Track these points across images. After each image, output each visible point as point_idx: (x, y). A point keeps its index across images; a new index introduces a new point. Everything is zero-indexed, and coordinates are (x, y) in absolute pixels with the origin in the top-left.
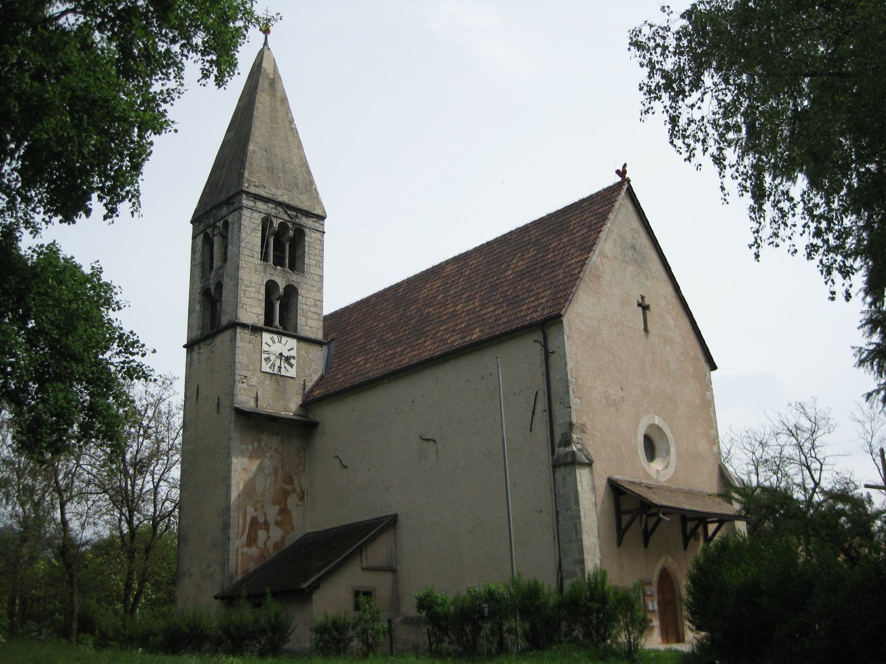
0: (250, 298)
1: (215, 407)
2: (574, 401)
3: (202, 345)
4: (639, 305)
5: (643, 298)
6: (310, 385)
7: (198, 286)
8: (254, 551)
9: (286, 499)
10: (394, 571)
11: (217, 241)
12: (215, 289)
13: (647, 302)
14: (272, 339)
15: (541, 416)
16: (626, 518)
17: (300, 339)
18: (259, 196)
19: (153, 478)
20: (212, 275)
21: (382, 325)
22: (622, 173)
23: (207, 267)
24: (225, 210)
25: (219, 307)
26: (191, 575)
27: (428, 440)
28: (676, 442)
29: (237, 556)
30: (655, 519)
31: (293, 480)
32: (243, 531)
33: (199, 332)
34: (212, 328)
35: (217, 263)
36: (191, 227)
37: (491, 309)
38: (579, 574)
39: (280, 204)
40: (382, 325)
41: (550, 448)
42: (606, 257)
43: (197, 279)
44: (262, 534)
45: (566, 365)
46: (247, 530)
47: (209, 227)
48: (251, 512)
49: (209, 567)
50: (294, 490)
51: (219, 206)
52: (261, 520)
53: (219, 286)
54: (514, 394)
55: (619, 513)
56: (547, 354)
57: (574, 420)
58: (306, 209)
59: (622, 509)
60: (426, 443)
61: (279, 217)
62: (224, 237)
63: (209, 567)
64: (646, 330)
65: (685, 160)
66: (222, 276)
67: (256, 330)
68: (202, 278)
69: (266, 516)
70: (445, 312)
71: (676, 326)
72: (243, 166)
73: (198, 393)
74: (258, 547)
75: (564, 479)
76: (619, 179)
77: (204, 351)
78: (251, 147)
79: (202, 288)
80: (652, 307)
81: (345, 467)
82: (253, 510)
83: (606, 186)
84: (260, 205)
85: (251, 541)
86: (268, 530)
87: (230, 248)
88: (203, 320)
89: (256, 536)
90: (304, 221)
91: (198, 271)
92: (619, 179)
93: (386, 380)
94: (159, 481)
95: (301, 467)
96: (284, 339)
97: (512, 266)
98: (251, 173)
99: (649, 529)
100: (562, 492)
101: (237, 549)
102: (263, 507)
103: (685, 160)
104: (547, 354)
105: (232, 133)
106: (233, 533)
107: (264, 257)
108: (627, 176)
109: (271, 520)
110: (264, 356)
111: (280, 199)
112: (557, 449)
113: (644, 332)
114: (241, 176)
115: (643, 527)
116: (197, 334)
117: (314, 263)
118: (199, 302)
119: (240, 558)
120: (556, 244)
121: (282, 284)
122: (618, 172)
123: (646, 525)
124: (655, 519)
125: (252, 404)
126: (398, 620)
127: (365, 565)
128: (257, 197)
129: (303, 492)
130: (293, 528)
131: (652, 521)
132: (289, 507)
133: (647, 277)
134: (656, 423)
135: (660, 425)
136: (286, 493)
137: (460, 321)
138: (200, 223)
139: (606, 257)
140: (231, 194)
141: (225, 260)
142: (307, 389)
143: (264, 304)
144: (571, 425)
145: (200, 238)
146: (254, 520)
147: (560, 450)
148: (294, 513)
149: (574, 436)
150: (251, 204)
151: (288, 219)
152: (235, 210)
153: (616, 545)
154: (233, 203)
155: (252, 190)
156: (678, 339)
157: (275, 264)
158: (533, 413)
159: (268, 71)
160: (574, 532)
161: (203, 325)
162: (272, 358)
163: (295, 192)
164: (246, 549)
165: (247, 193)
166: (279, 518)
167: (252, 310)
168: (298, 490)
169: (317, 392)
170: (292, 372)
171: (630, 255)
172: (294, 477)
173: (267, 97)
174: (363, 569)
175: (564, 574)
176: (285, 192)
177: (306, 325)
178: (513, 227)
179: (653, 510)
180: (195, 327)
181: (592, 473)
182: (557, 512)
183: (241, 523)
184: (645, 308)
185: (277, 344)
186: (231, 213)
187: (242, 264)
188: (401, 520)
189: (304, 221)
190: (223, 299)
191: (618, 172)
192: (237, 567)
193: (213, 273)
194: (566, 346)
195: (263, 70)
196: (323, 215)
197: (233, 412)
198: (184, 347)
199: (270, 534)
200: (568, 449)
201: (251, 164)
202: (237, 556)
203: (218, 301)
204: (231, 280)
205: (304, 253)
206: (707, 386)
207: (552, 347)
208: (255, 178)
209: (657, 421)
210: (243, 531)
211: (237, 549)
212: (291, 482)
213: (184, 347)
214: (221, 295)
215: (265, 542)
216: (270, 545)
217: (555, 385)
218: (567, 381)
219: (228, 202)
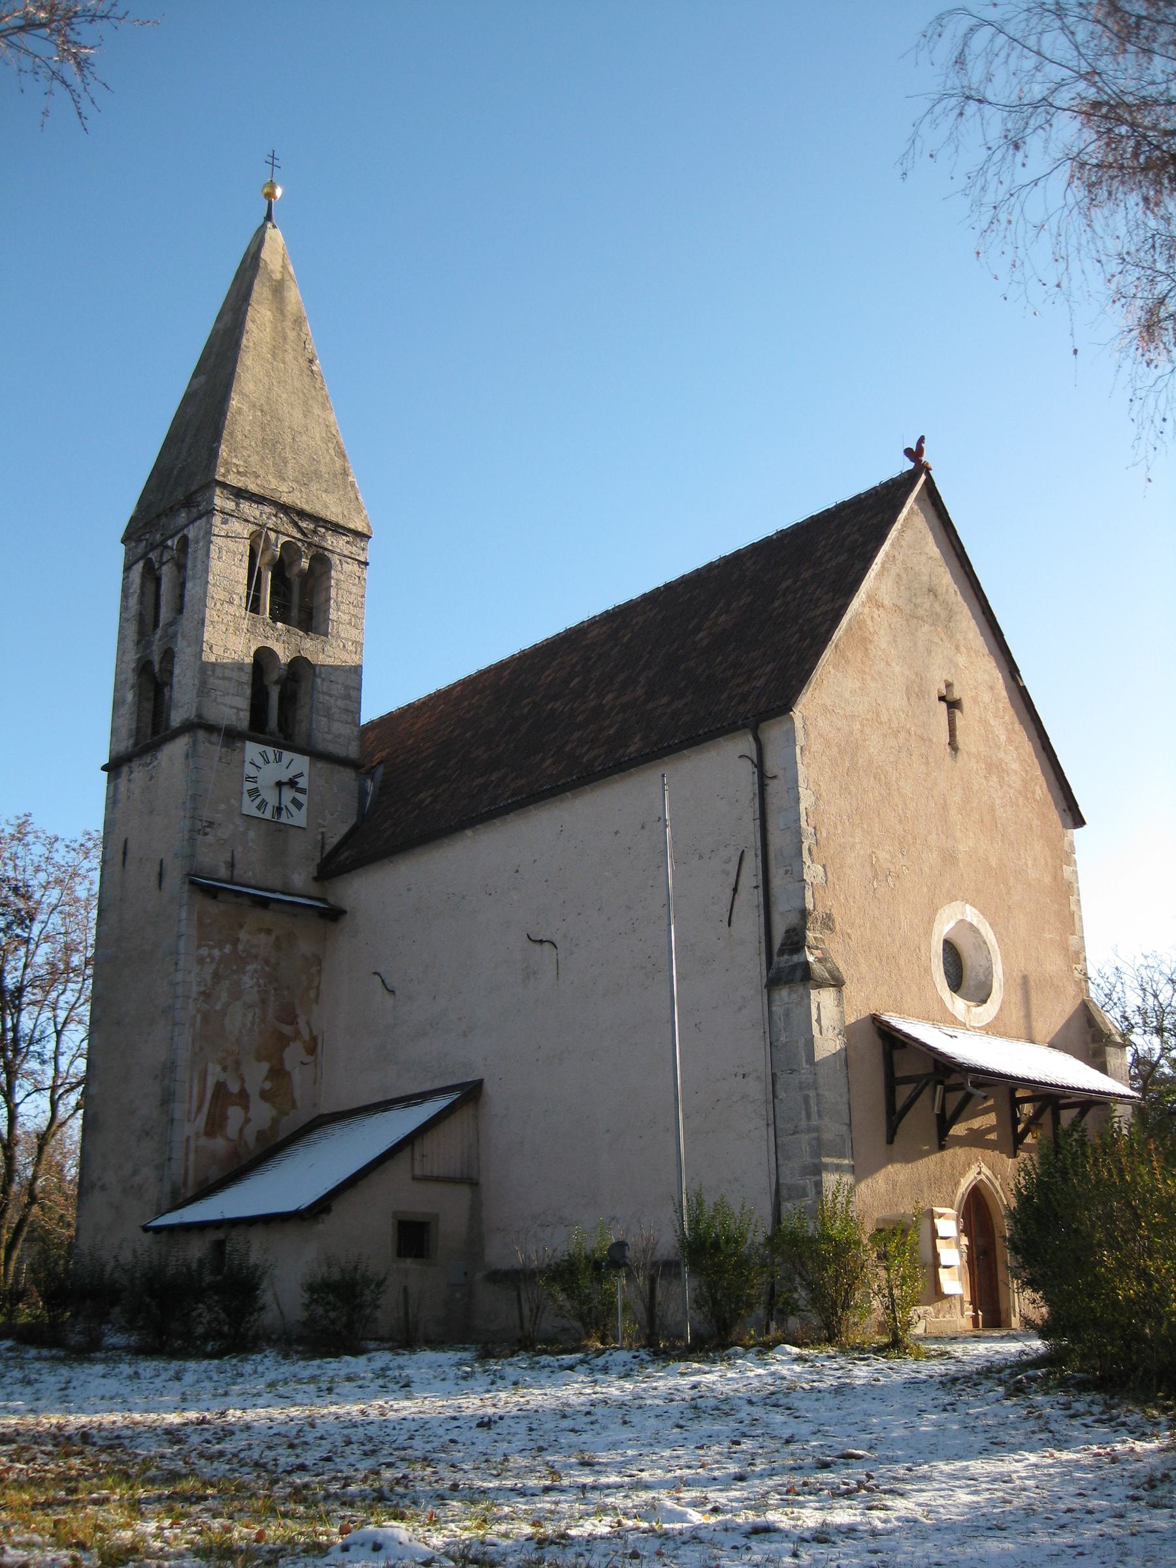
0: (224, 678)
1: (154, 879)
2: (812, 872)
3: (135, 764)
4: (942, 698)
5: (949, 685)
6: (333, 840)
7: (132, 656)
8: (219, 1144)
9: (282, 1050)
10: (473, 1183)
11: (167, 573)
12: (161, 662)
13: (957, 694)
14: (263, 755)
15: (749, 896)
16: (903, 1093)
17: (317, 755)
18: (247, 491)
19: (55, 1017)
20: (157, 636)
21: (468, 735)
22: (915, 454)
23: (149, 620)
24: (183, 517)
25: (167, 694)
26: (103, 1188)
27: (541, 942)
28: (1005, 956)
29: (187, 1154)
30: (960, 1095)
31: (296, 1016)
32: (200, 1108)
33: (131, 741)
34: (155, 732)
35: (165, 614)
36: (122, 548)
37: (664, 700)
38: (811, 1191)
39: (285, 509)
40: (468, 735)
41: (764, 957)
42: (879, 605)
43: (130, 644)
44: (235, 1114)
45: (797, 800)
46: (207, 1104)
48: (215, 1073)
49: (135, 1172)
50: (298, 1033)
51: (172, 511)
52: (234, 1088)
53: (169, 656)
54: (701, 857)
55: (891, 1082)
56: (763, 779)
57: (810, 906)
58: (334, 519)
59: (898, 1074)
60: (537, 947)
61: (284, 531)
62: (181, 567)
63: (135, 1172)
64: (953, 745)
67: (232, 737)
68: (138, 642)
69: (243, 1081)
70: (583, 708)
71: (1009, 740)
72: (217, 437)
73: (125, 853)
74: (228, 1139)
75: (787, 1015)
76: (910, 465)
77: (138, 773)
78: (235, 402)
79: (139, 659)
80: (966, 704)
81: (392, 992)
82: (218, 1068)
83: (885, 479)
84: (249, 509)
85: (215, 1125)
86: (246, 1108)
87: (189, 585)
88: (139, 720)
89: (225, 1118)
90: (335, 543)
91: (132, 629)
92: (910, 465)
93: (469, 833)
94: (65, 1023)
95: (312, 994)
96: (287, 755)
97: (708, 624)
98: (233, 450)
99: (949, 1114)
100: (783, 1039)
101: (188, 1138)
102: (238, 1064)
104: (763, 779)
105: (202, 379)
106: (179, 1110)
107: (254, 606)
108: (924, 459)
109: (253, 1091)
110: (249, 786)
111: (285, 499)
112: (775, 958)
113: (948, 749)
114: (213, 454)
115: (937, 1111)
116: (126, 744)
117: (346, 618)
118: (133, 687)
119: (192, 1157)
120: (789, 582)
121: (285, 656)
122: (908, 452)
123: (943, 1108)
124: (960, 1095)
125: (223, 872)
126: (479, 1276)
127: (418, 1171)
128: (240, 494)
129: (314, 1039)
130: (294, 1106)
131: (954, 1099)
132: (288, 1067)
133: (957, 648)
134: (969, 919)
135: (975, 923)
136: (283, 1041)
137: (607, 723)
138: (139, 540)
139: (879, 605)
140: (194, 488)
141: (180, 609)
142: (328, 848)
143: (248, 692)
144: (804, 914)
145: (139, 567)
146: (220, 1087)
147: (783, 961)
148: (297, 1077)
149: (810, 935)
150: (230, 505)
151: (299, 536)
152: (200, 517)
153: (883, 1140)
155: (233, 480)
156: (1015, 766)
157: (275, 618)
158: (735, 890)
159: (271, 267)
160: (803, 1114)
161: (138, 728)
163: (314, 487)
164: (203, 1141)
165: (224, 485)
166: (268, 1085)
167: (228, 700)
168: (306, 1037)
169: (346, 854)
170: (299, 818)
171: (927, 606)
172: (299, 1011)
173: (269, 313)
174: (414, 1178)
175: (784, 1193)
176: (295, 485)
178: (713, 557)
179: (954, 1080)
180: (124, 732)
181: (840, 1002)
182: (774, 1075)
183: (196, 1090)
184: (953, 705)
185: (273, 765)
186: (192, 522)
187: (210, 614)
188: (488, 1087)
189: (335, 543)
190: (175, 680)
191: (908, 452)
192: (186, 1173)
193: (159, 632)
194: (799, 765)
195: (262, 264)
196: (365, 531)
197: (186, 887)
198: (104, 768)
199: (251, 1114)
200: (796, 958)
201: (231, 434)
202: (187, 1154)
203: (166, 684)
204: (189, 646)
205: (328, 599)
206: (1066, 856)
207: (771, 766)
208: (238, 459)
209: (972, 915)
210: (200, 1108)
211: (188, 1138)
212: (292, 1020)
213: (104, 768)
214: (171, 673)
215: (241, 1130)
217: (777, 839)
218: (798, 833)
219: (189, 502)
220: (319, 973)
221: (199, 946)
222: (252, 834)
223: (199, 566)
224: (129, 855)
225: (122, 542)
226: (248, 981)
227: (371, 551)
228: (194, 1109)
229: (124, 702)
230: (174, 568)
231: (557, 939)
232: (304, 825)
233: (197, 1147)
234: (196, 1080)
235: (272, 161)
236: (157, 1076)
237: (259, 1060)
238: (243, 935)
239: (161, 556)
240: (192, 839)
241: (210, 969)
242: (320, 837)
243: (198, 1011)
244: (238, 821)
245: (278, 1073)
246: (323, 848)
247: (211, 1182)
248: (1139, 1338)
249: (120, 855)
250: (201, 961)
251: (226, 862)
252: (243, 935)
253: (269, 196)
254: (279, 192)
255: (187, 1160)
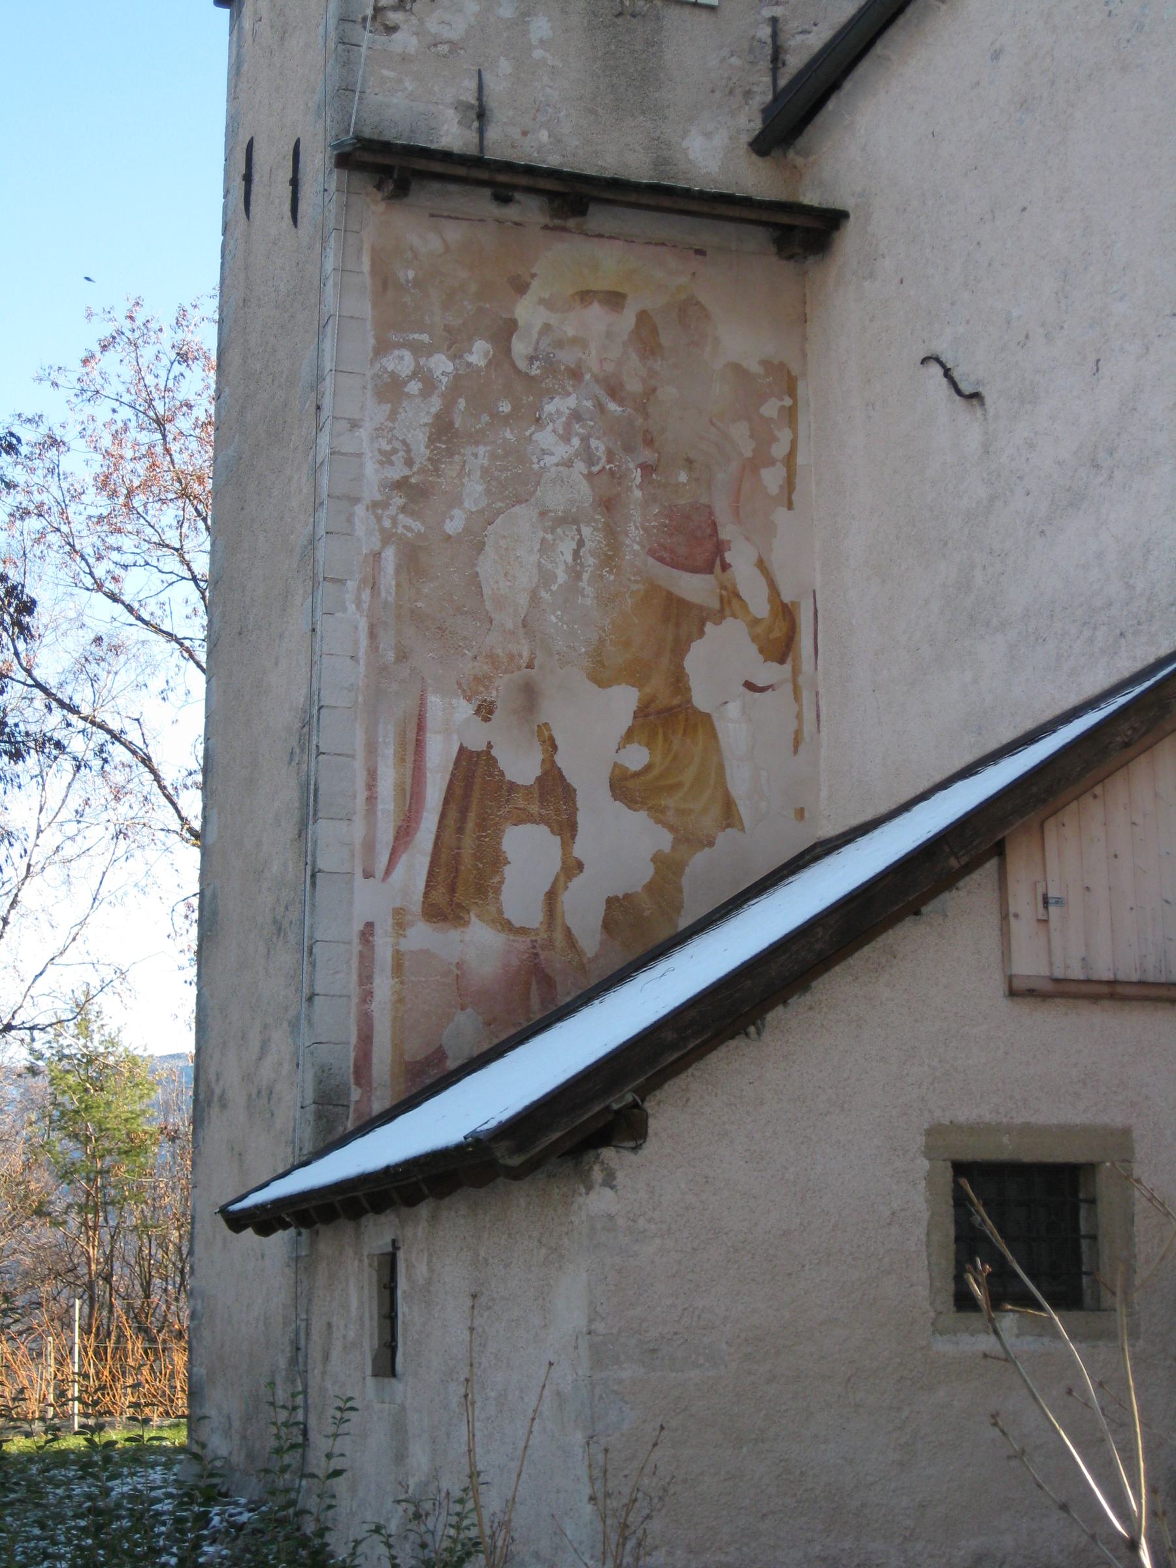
50: (730, 601)
95: (772, 478)
129: (786, 613)
132: (701, 700)
136: (680, 621)
168: (760, 606)
212: (711, 557)
220: (791, 415)
238: (528, 312)
250: (391, 390)
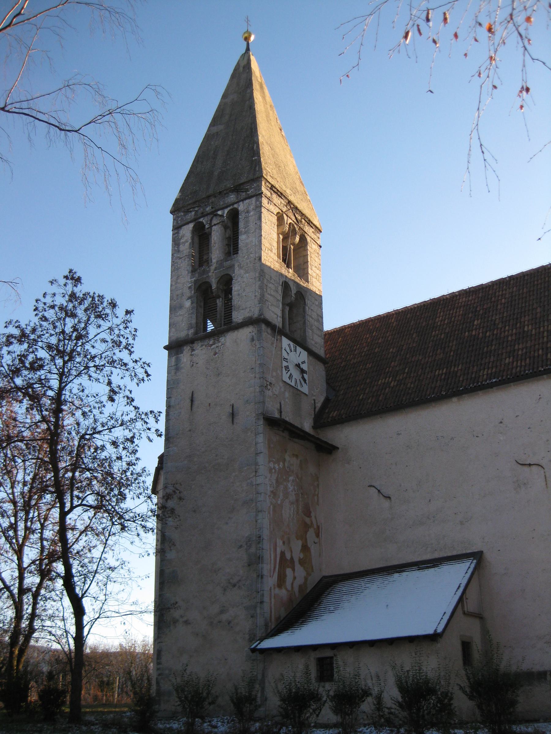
7: (187, 280)
8: (283, 593)
9: (306, 535)
27: (530, 465)
29: (271, 599)
31: (310, 512)
32: (275, 568)
35: (216, 253)
36: (171, 217)
46: (277, 567)
47: (203, 215)
60: (526, 469)
65: (149, 366)
66: (232, 267)
73: (192, 401)
79: (195, 282)
89: (285, 576)
93: (455, 399)
101: (271, 589)
103: (149, 366)
110: (285, 364)
111: (292, 198)
119: (273, 600)
129: (318, 527)
130: (313, 571)
132: (309, 545)
136: (306, 527)
142: (317, 409)
145: (187, 231)
151: (295, 221)
152: (250, 197)
154: (247, 190)
162: (291, 368)
164: (277, 591)
168: (315, 527)
172: (311, 510)
177: (312, 340)
183: (272, 558)
197: (261, 422)
198: (166, 348)
201: (263, 154)
202: (271, 599)
210: (275, 568)
213: (166, 348)
215: (292, 584)
216: (296, 589)
221: (269, 462)
222: (287, 394)
223: (252, 226)
224: (196, 403)
225: (172, 212)
226: (291, 487)
227: (322, 239)
228: (272, 568)
229: (181, 307)
230: (223, 228)
231: (543, 463)
232: (307, 393)
233: (275, 594)
234: (272, 550)
235: (248, 21)
236: (241, 546)
237: (298, 539)
239: (211, 220)
240: (262, 392)
241: (274, 476)
242: (313, 402)
243: (271, 503)
244: (281, 384)
245: (305, 548)
246: (315, 408)
247: (282, 619)
248: (269, 725)
249: (188, 401)
251: (277, 409)
252: (287, 458)
253: (247, 39)
254: (252, 38)
255: (271, 603)
